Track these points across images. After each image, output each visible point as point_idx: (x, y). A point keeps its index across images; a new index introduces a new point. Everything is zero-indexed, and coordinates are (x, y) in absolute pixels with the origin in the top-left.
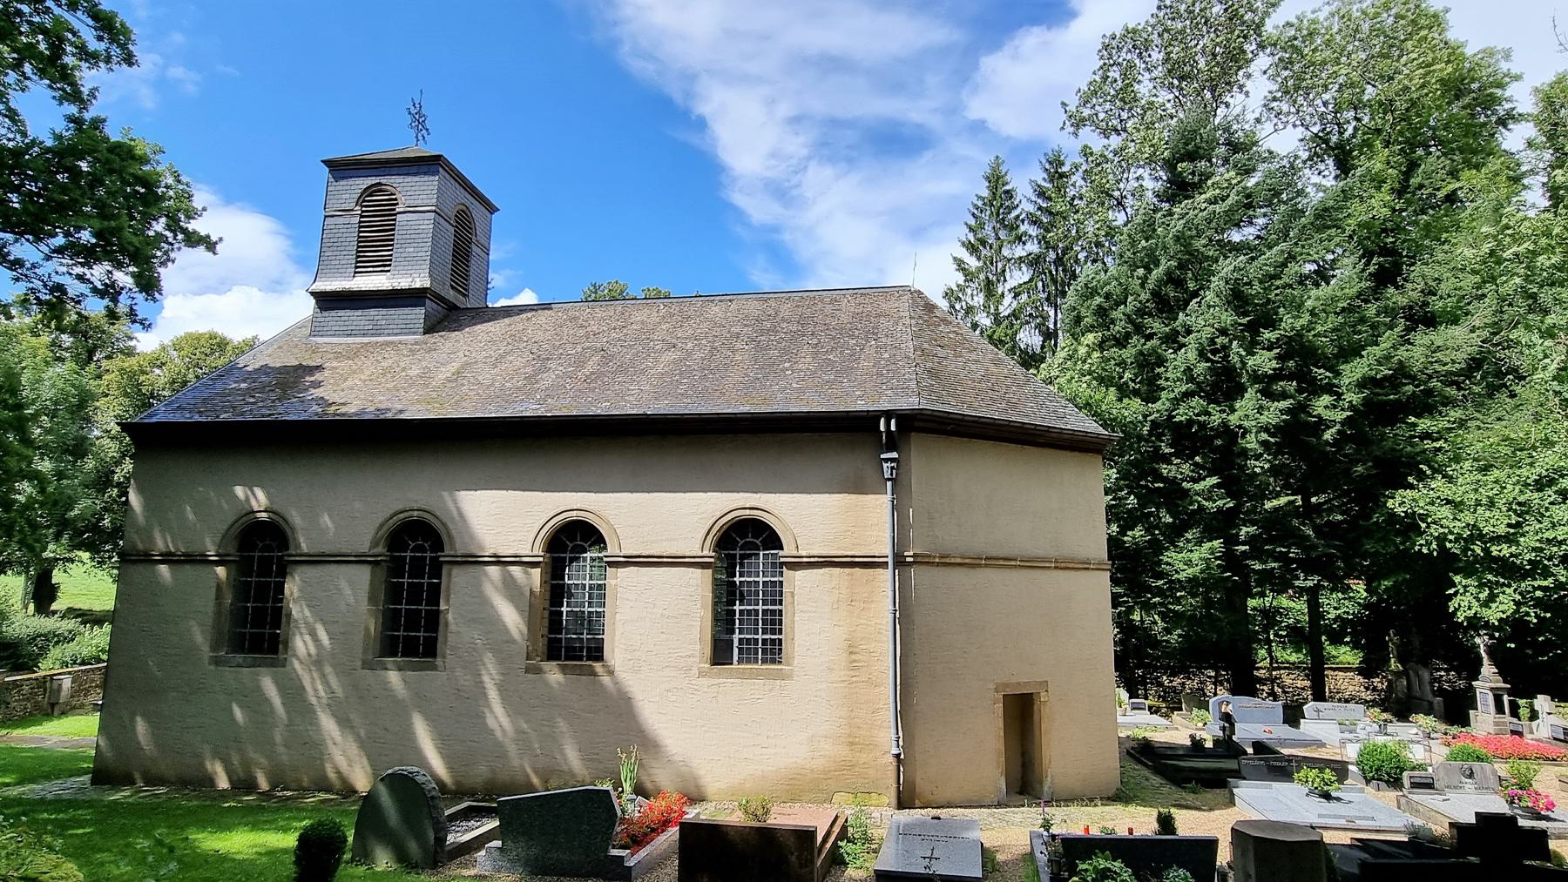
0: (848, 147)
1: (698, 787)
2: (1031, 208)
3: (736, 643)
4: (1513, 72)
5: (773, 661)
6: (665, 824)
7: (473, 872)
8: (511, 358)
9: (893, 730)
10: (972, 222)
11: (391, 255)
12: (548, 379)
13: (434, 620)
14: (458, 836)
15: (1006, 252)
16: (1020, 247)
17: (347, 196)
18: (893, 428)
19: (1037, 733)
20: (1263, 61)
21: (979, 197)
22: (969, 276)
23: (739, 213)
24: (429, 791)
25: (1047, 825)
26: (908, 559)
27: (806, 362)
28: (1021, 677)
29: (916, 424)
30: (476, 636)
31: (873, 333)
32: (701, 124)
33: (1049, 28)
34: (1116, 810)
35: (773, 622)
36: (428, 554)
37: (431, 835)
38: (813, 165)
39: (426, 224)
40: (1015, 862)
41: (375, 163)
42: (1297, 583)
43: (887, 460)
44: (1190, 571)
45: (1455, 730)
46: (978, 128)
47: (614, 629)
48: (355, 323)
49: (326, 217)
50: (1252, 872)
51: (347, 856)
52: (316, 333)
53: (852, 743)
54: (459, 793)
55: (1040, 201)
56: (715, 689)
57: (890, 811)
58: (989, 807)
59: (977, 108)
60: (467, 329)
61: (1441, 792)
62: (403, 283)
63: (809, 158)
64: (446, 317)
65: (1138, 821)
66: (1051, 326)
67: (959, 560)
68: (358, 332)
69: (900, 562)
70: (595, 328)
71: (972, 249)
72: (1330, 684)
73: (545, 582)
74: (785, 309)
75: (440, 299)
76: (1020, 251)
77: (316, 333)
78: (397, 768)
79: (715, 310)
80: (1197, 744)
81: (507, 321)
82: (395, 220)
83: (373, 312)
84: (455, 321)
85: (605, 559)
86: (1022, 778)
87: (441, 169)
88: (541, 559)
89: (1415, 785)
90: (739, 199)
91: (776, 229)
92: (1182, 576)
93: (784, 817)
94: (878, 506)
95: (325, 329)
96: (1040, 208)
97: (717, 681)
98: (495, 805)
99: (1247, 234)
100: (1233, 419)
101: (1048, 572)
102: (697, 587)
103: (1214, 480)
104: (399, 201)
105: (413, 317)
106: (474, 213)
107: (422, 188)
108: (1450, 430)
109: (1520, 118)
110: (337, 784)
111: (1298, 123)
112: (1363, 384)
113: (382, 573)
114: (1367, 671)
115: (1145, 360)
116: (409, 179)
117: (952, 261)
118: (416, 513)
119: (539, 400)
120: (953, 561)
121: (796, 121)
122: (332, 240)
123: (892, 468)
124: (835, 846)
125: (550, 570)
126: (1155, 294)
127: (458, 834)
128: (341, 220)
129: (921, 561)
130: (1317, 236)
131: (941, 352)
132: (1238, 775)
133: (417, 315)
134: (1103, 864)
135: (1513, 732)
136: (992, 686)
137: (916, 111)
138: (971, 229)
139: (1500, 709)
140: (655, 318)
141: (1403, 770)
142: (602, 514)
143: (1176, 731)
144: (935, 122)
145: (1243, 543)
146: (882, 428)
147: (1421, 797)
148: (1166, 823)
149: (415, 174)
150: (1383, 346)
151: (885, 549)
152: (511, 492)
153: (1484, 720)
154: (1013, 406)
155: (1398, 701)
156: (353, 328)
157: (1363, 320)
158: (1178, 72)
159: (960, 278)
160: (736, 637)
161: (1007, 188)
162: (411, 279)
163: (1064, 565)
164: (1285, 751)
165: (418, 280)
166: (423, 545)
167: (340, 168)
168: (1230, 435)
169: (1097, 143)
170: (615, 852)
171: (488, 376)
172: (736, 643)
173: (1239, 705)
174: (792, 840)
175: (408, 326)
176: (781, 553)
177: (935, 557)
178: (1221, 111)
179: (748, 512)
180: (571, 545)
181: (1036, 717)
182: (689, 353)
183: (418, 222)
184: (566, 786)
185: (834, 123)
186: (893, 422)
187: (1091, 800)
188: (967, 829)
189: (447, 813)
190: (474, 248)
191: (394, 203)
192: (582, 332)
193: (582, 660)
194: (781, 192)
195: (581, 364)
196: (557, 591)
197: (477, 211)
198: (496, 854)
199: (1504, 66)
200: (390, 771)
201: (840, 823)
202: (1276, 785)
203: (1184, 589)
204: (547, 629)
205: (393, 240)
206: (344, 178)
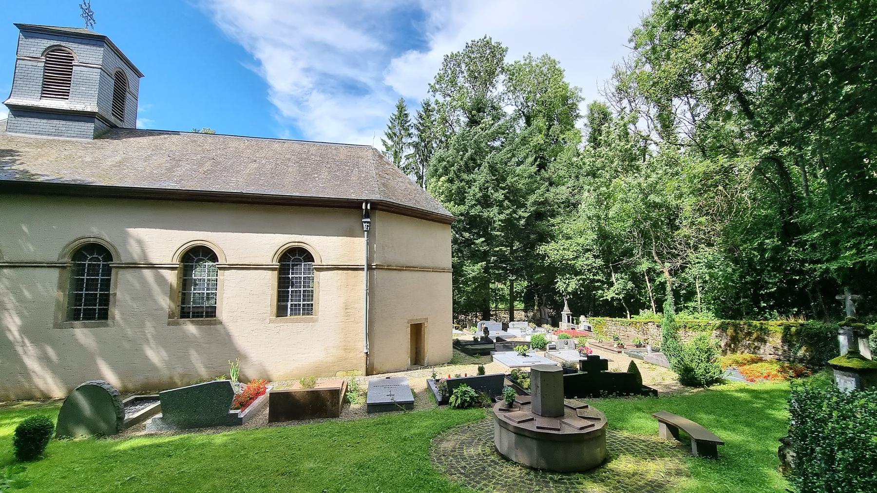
0: (333, 87)
1: (267, 375)
2: (416, 122)
3: (289, 306)
4: (582, 97)
5: (308, 314)
6: (258, 394)
7: (143, 433)
8: (155, 158)
9: (365, 342)
10: (390, 125)
11: (69, 90)
12: (179, 172)
13: (105, 300)
14: (131, 414)
15: (403, 140)
16: (410, 138)
17: (35, 49)
18: (369, 208)
19: (423, 339)
20: (502, 77)
21: (393, 115)
22: (388, 149)
23: (277, 110)
24: (113, 393)
25: (434, 376)
26: (373, 267)
27: (325, 174)
28: (417, 318)
29: (379, 207)
30: (135, 307)
31: (357, 165)
32: (259, 63)
33: (420, 52)
34: (453, 367)
35: (308, 296)
36: (101, 263)
37: (115, 417)
38: (315, 92)
39: (96, 75)
40: (422, 392)
41: (58, 33)
42: (509, 278)
43: (365, 222)
44: (473, 274)
45: (556, 329)
46: (389, 89)
47: (222, 302)
48: (41, 127)
49: (17, 59)
50: (539, 386)
51: (54, 435)
52: (10, 130)
53: (345, 349)
54: (125, 392)
55: (420, 120)
56: (278, 328)
57: (363, 377)
58: (404, 371)
59: (390, 81)
60: (124, 139)
61: (558, 351)
62: (79, 107)
63: (313, 89)
64: (107, 132)
65: (470, 370)
66: (421, 173)
67: (395, 268)
68: (44, 133)
69: (370, 268)
70: (207, 147)
71: (390, 137)
72: (515, 316)
73: (180, 278)
74: (313, 150)
75: (106, 121)
76: (410, 140)
77: (10, 130)
78: (88, 382)
79: (276, 146)
80: (476, 340)
81: (151, 138)
82: (72, 69)
83: (55, 122)
84: (116, 134)
85: (217, 266)
86: (416, 358)
87: (105, 45)
88: (178, 266)
89: (550, 349)
90: (277, 102)
91: (295, 120)
92: (470, 276)
93: (324, 384)
94: (361, 243)
95: (18, 128)
96: (420, 123)
97: (279, 325)
98: (158, 395)
99: (497, 144)
100: (491, 215)
101: (429, 273)
102: (271, 279)
103: (483, 239)
104: (75, 58)
105: (86, 128)
106: (127, 74)
107: (91, 53)
108: (560, 223)
109: (581, 117)
110: (38, 395)
111: (514, 104)
112: (535, 203)
113: (67, 274)
114: (526, 310)
115: (460, 190)
116: (82, 46)
117: (381, 141)
118: (92, 239)
119: (176, 181)
120: (392, 268)
121: (308, 70)
122: (23, 74)
123: (368, 226)
124: (345, 395)
125: (182, 272)
126: (466, 163)
127: (130, 414)
128: (30, 63)
129: (379, 268)
130: (522, 147)
131: (387, 177)
132: (494, 350)
133: (89, 127)
134: (464, 389)
135: (572, 329)
136: (406, 321)
137: (364, 77)
138: (389, 128)
139: (569, 321)
140: (242, 146)
141: (545, 344)
142: (216, 243)
143: (467, 335)
144: (371, 83)
145: (492, 263)
146: (364, 207)
147: (552, 353)
148: (481, 370)
149: (87, 44)
150: (542, 190)
151: (363, 262)
152: (158, 230)
153: (564, 325)
154: (418, 202)
155: (538, 320)
156: (41, 130)
157: (536, 181)
158: (473, 77)
159: (384, 149)
160: (289, 304)
161: (406, 112)
162: (84, 106)
163: (435, 270)
164: (508, 340)
165: (89, 107)
166: (97, 258)
167: (29, 31)
168: (489, 222)
169: (441, 99)
170: (232, 412)
171: (141, 166)
172: (289, 306)
173: (487, 324)
174: (328, 396)
175: (82, 133)
176: (313, 263)
178: (489, 94)
179: (296, 244)
180: (196, 259)
181: (423, 333)
182: (264, 165)
183: (88, 73)
184: (201, 382)
185: (325, 75)
186: (369, 205)
187: (443, 364)
188: (403, 381)
189: (124, 401)
190: (128, 94)
191: (71, 59)
192: (200, 149)
193: (202, 317)
194: (298, 102)
195: (201, 165)
196: (186, 281)
197: (129, 74)
198: (159, 422)
199: (580, 94)
200: (83, 384)
201: (345, 384)
202: (507, 353)
203: (471, 281)
204: (180, 302)
205: (70, 81)
206: (32, 37)
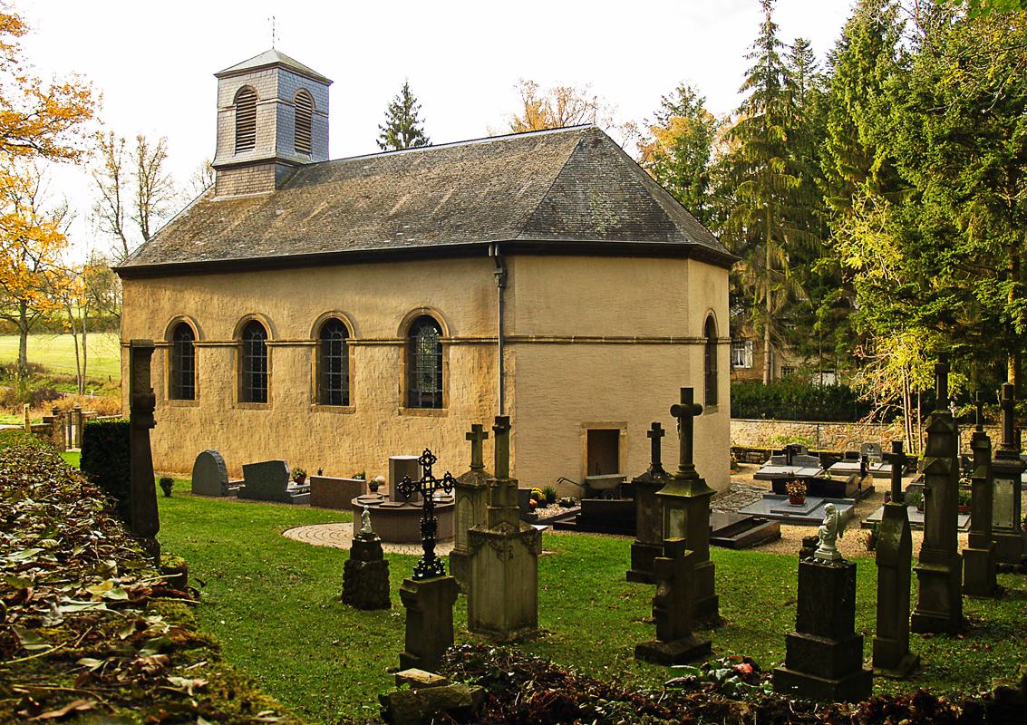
136: (579, 424)
177: (532, 338)
197: (314, 88)
